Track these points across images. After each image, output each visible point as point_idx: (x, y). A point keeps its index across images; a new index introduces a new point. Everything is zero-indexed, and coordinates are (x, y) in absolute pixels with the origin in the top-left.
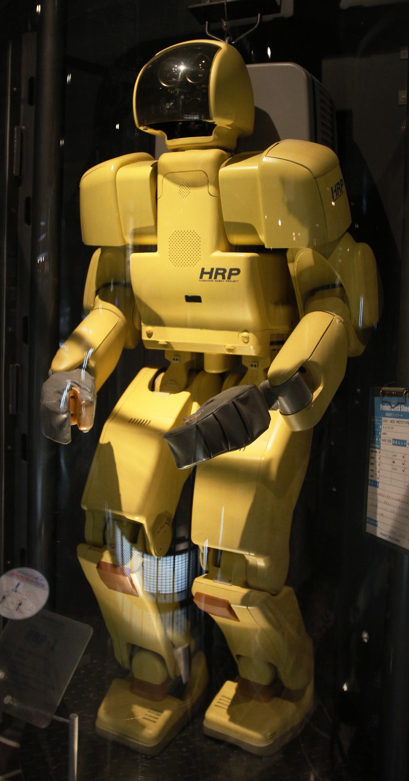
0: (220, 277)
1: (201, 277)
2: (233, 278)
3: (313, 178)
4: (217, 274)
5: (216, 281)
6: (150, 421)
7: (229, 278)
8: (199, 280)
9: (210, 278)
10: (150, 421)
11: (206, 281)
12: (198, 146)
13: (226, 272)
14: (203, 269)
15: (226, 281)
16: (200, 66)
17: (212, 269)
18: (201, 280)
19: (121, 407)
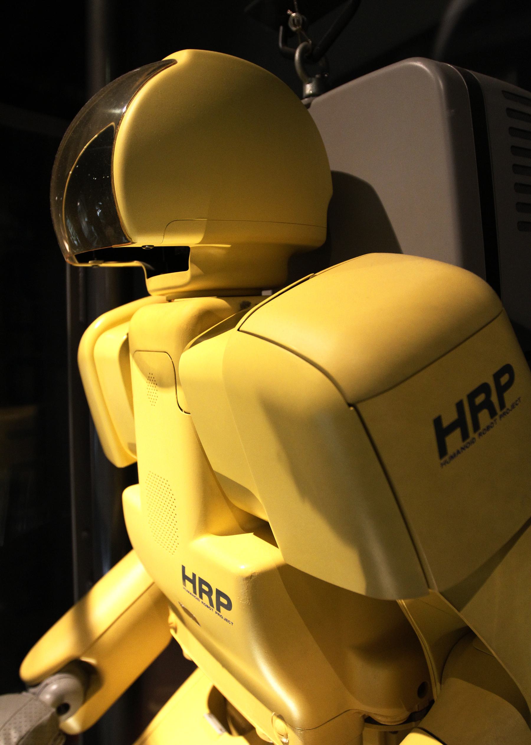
0: (484, 416)
1: (442, 451)
2: (509, 397)
3: (346, 406)
4: (475, 410)
5: (480, 435)
6: (183, 568)
7: (502, 405)
8: (442, 465)
9: (465, 436)
10: (183, 568)
11: (458, 452)
12: (176, 293)
13: (213, 594)
14: (438, 422)
15: (501, 416)
16: (95, 179)
17: (460, 406)
18: (447, 458)
19: (164, 237)
